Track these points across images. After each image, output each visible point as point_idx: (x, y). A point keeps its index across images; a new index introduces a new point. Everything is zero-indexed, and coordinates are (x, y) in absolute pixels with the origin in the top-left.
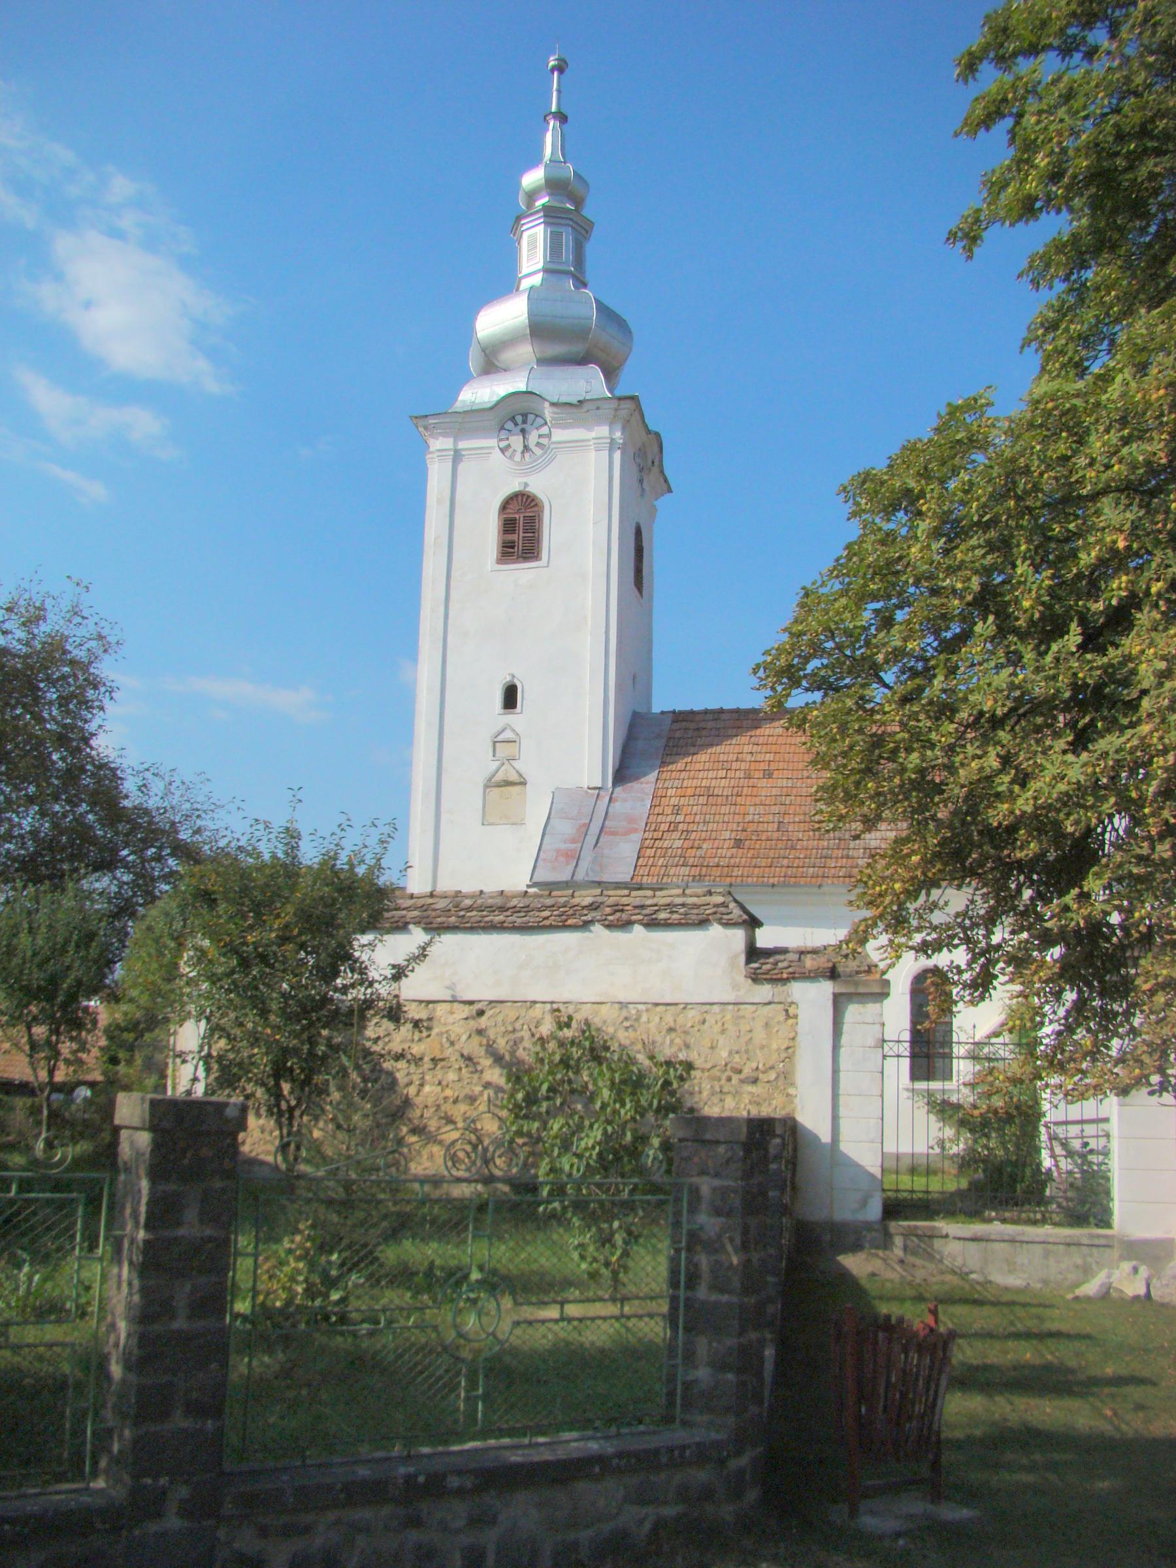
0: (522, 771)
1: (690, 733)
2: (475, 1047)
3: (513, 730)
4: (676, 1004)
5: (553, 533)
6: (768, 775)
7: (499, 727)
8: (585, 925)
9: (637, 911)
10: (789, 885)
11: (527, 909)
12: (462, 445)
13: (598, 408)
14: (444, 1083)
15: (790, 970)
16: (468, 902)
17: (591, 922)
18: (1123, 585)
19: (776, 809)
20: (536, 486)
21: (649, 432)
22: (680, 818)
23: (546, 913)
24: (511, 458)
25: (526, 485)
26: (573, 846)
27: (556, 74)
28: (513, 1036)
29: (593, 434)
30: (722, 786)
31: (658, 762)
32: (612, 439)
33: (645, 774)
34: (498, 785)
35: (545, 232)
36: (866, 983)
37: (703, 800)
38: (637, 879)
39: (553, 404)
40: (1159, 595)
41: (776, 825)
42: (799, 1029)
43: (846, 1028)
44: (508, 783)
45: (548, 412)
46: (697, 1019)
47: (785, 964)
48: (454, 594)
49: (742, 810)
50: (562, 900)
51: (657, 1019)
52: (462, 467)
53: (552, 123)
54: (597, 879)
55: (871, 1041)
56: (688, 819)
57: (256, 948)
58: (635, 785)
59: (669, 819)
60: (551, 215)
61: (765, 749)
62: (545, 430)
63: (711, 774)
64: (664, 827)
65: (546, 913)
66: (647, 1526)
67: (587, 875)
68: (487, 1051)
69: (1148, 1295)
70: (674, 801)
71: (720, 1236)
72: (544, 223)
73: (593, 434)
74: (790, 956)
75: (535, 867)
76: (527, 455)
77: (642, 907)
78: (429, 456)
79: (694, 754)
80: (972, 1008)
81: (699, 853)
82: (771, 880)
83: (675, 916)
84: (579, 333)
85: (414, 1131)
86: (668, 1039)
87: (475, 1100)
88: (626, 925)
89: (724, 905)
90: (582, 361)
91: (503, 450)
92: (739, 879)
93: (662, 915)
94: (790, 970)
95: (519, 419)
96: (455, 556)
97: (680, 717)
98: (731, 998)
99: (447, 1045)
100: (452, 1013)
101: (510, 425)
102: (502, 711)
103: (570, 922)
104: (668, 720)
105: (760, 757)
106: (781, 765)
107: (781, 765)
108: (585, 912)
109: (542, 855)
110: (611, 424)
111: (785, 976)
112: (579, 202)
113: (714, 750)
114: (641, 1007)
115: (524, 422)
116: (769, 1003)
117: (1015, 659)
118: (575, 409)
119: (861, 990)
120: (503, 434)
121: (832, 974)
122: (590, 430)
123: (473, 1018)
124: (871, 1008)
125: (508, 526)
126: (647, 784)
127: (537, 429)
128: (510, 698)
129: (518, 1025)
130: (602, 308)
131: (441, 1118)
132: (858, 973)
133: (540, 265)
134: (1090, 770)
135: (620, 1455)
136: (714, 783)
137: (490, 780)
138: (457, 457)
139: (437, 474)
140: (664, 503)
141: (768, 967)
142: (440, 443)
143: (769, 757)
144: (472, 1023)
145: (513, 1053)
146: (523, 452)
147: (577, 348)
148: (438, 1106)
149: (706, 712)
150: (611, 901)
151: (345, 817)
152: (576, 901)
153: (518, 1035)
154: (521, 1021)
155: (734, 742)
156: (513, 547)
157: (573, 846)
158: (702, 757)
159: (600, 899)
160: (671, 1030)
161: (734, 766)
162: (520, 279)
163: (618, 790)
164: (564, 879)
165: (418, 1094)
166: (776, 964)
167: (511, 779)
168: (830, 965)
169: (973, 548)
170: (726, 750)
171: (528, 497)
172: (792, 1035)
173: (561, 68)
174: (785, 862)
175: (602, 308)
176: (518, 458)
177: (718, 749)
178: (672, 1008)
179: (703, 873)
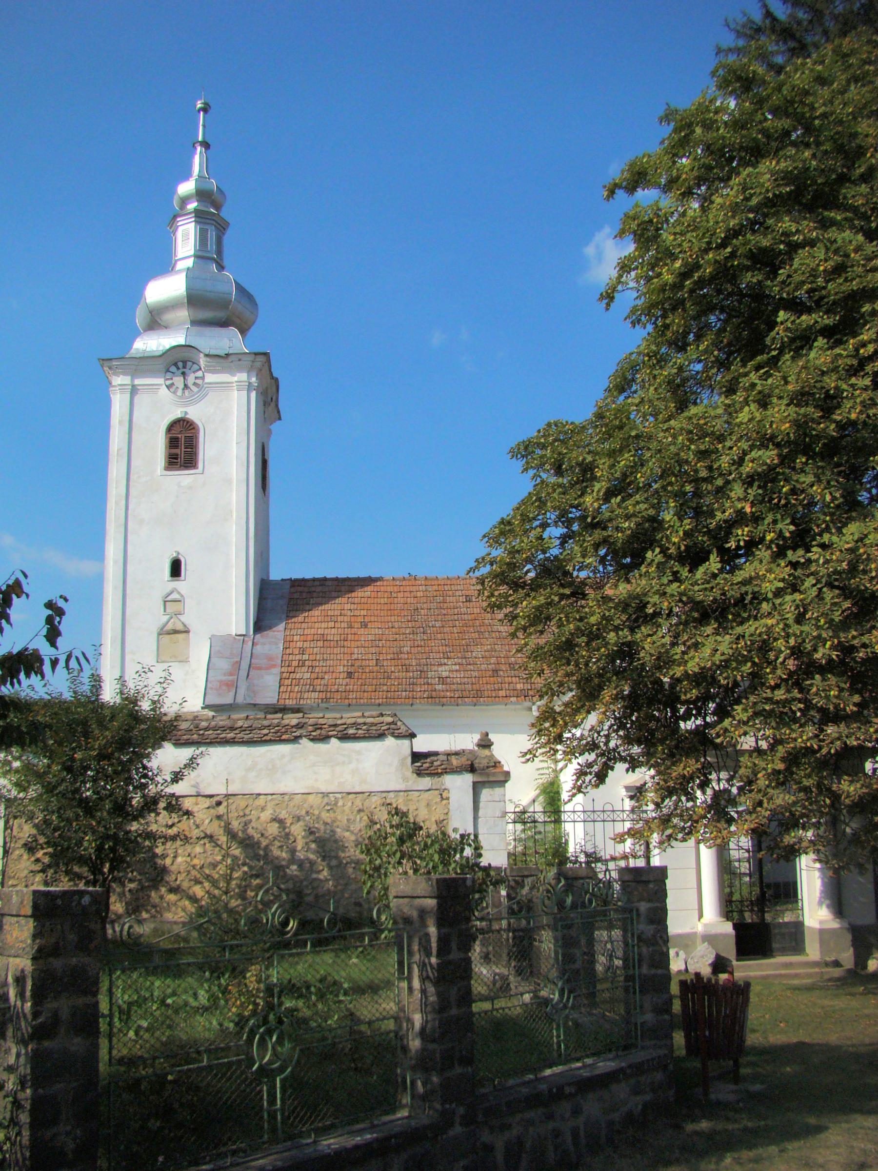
0: (187, 623)
1: (305, 595)
2: (215, 828)
3: (179, 593)
4: (363, 793)
5: (207, 449)
6: (365, 625)
7: (168, 590)
8: (296, 739)
9: (332, 729)
10: (390, 705)
11: (251, 729)
12: (137, 382)
13: (240, 360)
14: (193, 855)
15: (443, 767)
16: (204, 724)
17: (300, 737)
18: (745, 533)
19: (373, 650)
20: (194, 414)
21: (272, 377)
22: (306, 657)
23: (266, 731)
24: (175, 393)
25: (186, 413)
26: (231, 678)
27: (202, 113)
28: (244, 819)
29: (236, 379)
30: (333, 634)
31: (284, 616)
32: (250, 383)
33: (276, 625)
34: (169, 634)
35: (196, 227)
36: (494, 774)
37: (320, 644)
38: (282, 702)
39: (207, 356)
40: (771, 541)
41: (374, 662)
42: (451, 807)
43: (481, 805)
44: (176, 632)
45: (203, 361)
46: (378, 803)
47: (438, 763)
48: (131, 490)
49: (349, 651)
50: (276, 721)
51: (350, 804)
52: (137, 399)
53: (199, 149)
54: (252, 702)
55: (498, 814)
56: (312, 657)
57: (81, 763)
58: (270, 633)
59: (298, 657)
60: (200, 216)
61: (359, 607)
62: (199, 374)
63: (324, 625)
64: (295, 663)
65: (266, 731)
66: (640, 1107)
67: (245, 699)
68: (225, 831)
69: (686, 970)
70: (299, 644)
71: (654, 936)
72: (195, 221)
73: (236, 379)
74: (441, 757)
75: (205, 694)
76: (187, 392)
77: (336, 725)
78: (112, 389)
79: (309, 610)
80: (595, 790)
81: (323, 682)
82: (377, 701)
83: (360, 732)
84: (222, 303)
85: (171, 890)
86: (358, 817)
87: (217, 866)
88: (325, 739)
89: (393, 723)
90: (223, 324)
91: (168, 387)
92: (354, 701)
93: (351, 731)
94: (443, 767)
95: (180, 365)
96: (133, 464)
97: (297, 584)
98: (403, 787)
99: (194, 827)
100: (197, 804)
101: (173, 369)
102: (170, 578)
103: (284, 737)
104: (288, 586)
105: (357, 613)
106: (372, 619)
107: (372, 619)
108: (294, 730)
109: (209, 685)
110: (248, 372)
111: (440, 771)
112: (218, 207)
113: (323, 607)
114: (339, 796)
115: (184, 367)
116: (429, 790)
117: (676, 577)
118: (223, 360)
119: (491, 779)
120: (169, 375)
121: (472, 769)
122: (234, 375)
123: (213, 808)
124: (498, 791)
125: (173, 442)
126: (279, 631)
127: (194, 372)
128: (176, 569)
129: (247, 811)
130: (240, 288)
131: (191, 880)
132: (488, 767)
133: (192, 253)
134: (734, 646)
135: (630, 1066)
136: (326, 631)
137: (162, 629)
138: (134, 390)
139: (119, 403)
140: (276, 427)
141: (427, 765)
142: (118, 380)
143: (363, 613)
144: (212, 811)
145: (244, 831)
146: (183, 389)
147: (220, 314)
148: (189, 872)
149: (314, 580)
150: (311, 721)
151: (141, 666)
152: (286, 722)
153: (249, 818)
154: (249, 809)
155: (337, 601)
156: (177, 459)
157: (231, 678)
158: (316, 612)
159: (304, 721)
160: (360, 811)
161: (339, 619)
162: (176, 261)
163: (258, 636)
164: (229, 702)
165: (172, 864)
166: (432, 763)
167: (177, 629)
168: (469, 762)
169: (638, 503)
170: (333, 607)
171: (188, 422)
172: (446, 811)
173: (205, 110)
174: (385, 688)
175: (240, 288)
176: (180, 393)
177: (326, 607)
178: (361, 795)
179: (328, 696)
